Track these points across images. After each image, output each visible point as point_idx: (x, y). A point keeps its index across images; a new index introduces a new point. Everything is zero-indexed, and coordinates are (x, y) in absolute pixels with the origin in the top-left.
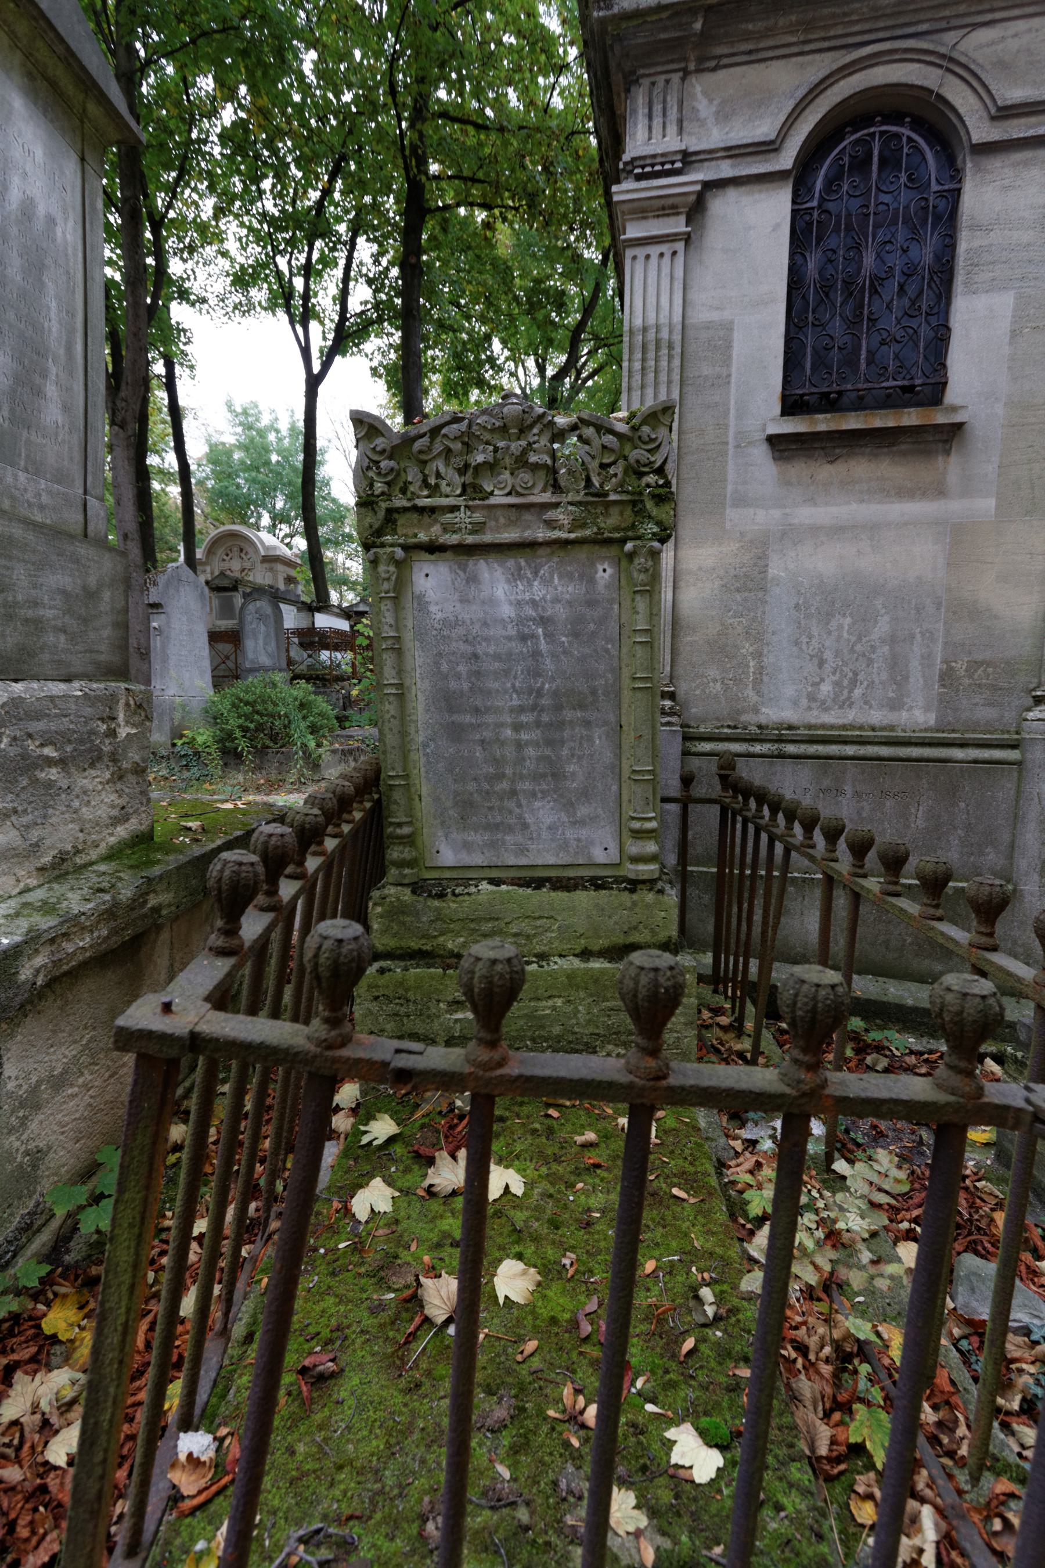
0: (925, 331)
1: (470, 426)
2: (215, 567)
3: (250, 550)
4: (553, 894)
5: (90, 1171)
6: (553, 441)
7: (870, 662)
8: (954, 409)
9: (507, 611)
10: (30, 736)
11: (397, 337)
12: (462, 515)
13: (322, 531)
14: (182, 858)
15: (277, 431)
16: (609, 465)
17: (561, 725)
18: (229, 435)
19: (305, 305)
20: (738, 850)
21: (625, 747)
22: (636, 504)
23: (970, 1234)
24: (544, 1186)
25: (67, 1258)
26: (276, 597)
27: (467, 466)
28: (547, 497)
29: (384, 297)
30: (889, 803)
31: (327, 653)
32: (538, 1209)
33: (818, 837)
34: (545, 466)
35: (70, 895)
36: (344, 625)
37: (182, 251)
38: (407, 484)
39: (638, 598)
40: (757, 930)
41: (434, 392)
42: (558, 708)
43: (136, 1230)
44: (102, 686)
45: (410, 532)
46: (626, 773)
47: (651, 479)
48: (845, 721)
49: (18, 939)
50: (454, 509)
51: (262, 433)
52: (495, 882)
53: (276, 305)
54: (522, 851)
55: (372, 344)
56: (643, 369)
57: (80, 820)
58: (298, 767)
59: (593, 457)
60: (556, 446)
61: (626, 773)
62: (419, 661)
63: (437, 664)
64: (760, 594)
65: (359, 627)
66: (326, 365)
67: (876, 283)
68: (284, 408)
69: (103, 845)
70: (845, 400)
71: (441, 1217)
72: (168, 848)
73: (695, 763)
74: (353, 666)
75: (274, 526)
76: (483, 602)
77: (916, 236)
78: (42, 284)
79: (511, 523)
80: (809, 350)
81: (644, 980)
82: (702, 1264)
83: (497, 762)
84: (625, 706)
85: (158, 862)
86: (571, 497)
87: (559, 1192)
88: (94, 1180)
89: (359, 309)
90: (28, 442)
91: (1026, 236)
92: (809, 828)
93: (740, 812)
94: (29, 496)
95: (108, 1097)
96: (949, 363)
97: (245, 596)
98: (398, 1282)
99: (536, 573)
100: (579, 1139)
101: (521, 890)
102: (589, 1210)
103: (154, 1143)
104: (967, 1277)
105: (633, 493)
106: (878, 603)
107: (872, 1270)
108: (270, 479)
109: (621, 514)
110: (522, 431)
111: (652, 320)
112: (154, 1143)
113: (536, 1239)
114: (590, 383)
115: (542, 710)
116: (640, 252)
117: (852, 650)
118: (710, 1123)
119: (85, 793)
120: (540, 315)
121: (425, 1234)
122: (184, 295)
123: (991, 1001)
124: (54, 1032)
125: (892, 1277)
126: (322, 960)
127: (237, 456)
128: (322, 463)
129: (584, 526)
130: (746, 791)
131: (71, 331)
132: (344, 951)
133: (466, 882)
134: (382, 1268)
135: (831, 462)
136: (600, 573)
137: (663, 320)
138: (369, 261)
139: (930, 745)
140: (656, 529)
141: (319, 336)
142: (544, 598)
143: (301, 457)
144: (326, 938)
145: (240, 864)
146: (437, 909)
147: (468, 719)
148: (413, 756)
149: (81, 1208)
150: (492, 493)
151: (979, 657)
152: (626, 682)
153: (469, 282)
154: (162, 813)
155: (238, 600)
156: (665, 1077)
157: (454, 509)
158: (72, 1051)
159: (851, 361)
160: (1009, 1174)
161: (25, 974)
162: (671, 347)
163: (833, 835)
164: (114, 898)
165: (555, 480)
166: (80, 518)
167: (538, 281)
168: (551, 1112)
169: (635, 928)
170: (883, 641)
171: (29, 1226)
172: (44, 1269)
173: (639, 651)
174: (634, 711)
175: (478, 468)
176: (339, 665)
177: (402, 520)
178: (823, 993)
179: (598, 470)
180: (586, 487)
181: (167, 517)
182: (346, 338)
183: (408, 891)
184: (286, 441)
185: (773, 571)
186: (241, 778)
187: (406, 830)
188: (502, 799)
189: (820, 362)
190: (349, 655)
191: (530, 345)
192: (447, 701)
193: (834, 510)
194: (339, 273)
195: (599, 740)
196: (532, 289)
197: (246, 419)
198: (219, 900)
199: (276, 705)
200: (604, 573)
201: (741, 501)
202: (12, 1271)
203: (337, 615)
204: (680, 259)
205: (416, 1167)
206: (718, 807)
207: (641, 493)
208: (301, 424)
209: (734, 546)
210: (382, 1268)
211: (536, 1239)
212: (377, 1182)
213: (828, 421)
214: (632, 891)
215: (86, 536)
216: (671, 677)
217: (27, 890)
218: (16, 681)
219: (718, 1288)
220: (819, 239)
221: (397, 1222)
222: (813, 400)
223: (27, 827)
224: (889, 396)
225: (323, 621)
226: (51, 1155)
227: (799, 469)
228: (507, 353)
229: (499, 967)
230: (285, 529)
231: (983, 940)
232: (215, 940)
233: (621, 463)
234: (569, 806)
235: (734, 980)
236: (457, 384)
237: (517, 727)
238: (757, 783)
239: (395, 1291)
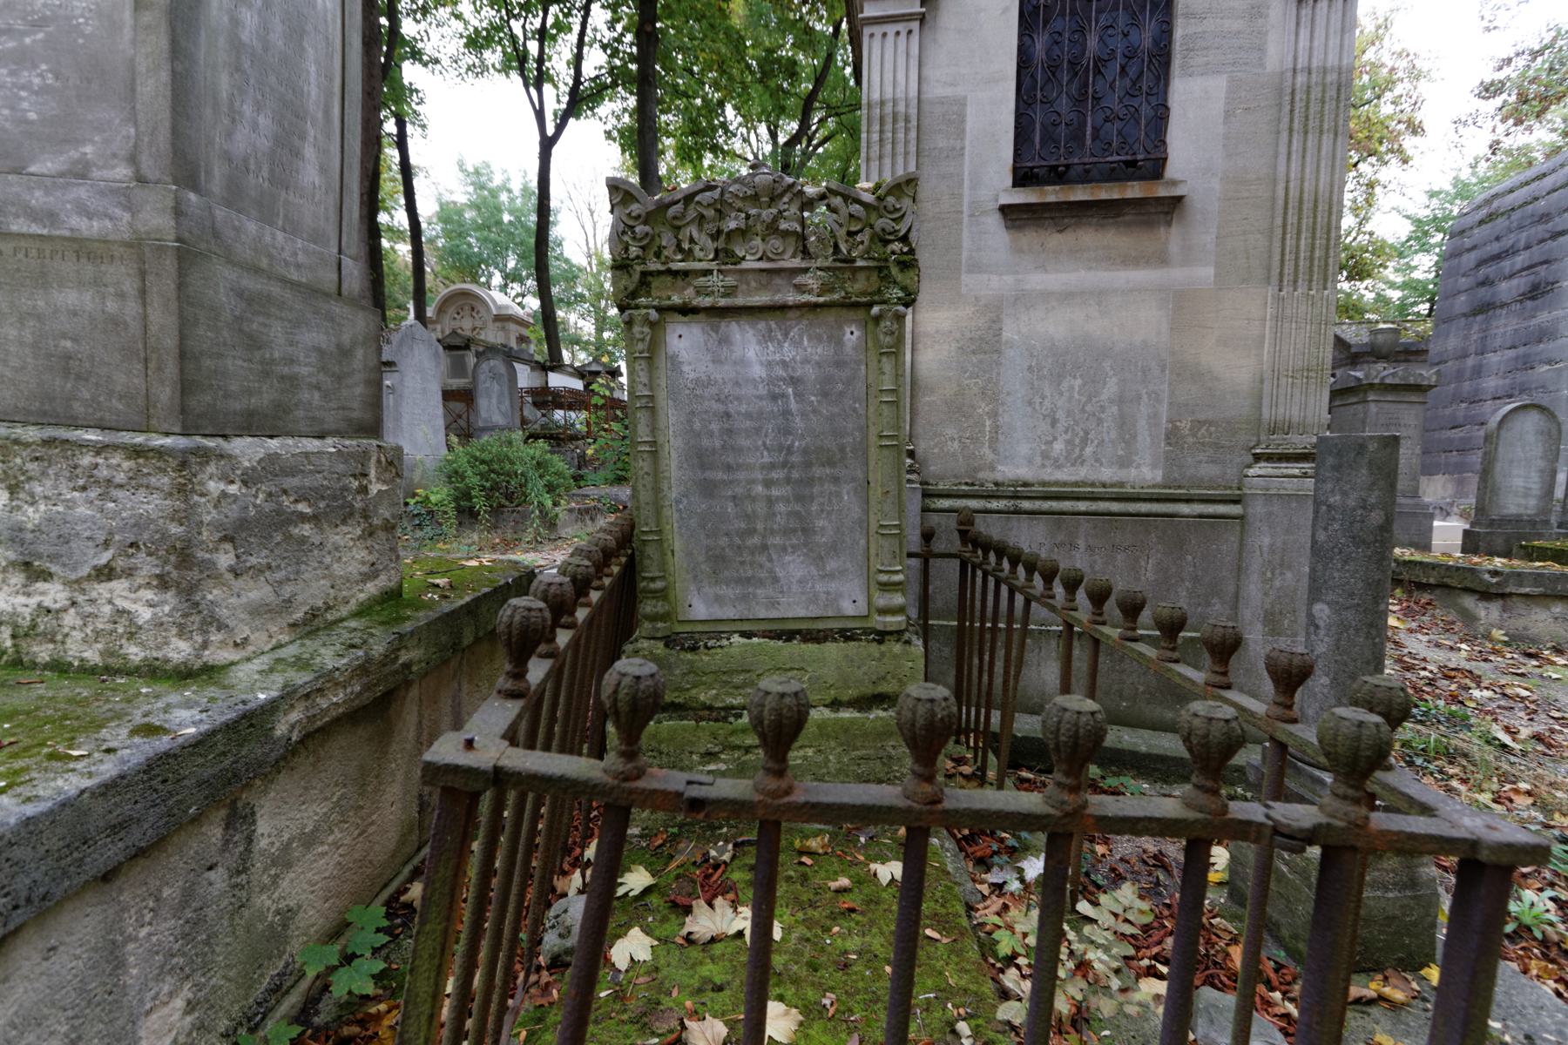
0: (1146, 111)
1: (722, 194)
2: (446, 326)
3: (482, 310)
5: (339, 930)
6: (802, 210)
7: (1100, 421)
8: (1174, 183)
9: (758, 371)
10: (285, 492)
11: (632, 102)
12: (715, 280)
13: (555, 290)
14: (433, 615)
15: (509, 191)
16: (856, 233)
17: (810, 482)
18: (461, 195)
19: (539, 69)
20: (978, 604)
21: (872, 502)
22: (881, 270)
23: (1207, 968)
24: (801, 930)
25: (317, 1020)
27: (719, 232)
28: (797, 262)
29: (618, 62)
30: (1120, 557)
31: (561, 412)
32: (796, 952)
33: (1058, 589)
34: (795, 233)
35: (323, 651)
36: (578, 385)
37: (415, 12)
38: (660, 249)
39: (884, 359)
40: (998, 681)
41: (670, 154)
42: (808, 465)
43: (436, 961)
44: (354, 443)
46: (873, 527)
47: (896, 246)
48: (1078, 478)
49: (274, 694)
51: (494, 194)
52: (747, 635)
53: (511, 68)
54: (774, 604)
55: (606, 108)
56: (881, 140)
57: (331, 576)
58: (534, 525)
59: (841, 225)
60: (806, 214)
61: (873, 527)
62: (672, 420)
63: (689, 421)
64: (995, 356)
65: (594, 386)
66: (560, 128)
67: (1100, 64)
68: (515, 168)
69: (353, 601)
70: (1072, 173)
71: (701, 963)
72: (417, 604)
73: (934, 519)
74: (588, 424)
75: (506, 285)
77: (1135, 22)
78: (303, 49)
79: (763, 287)
80: (1038, 126)
81: (921, 710)
82: (957, 1000)
83: (749, 518)
84: (872, 463)
85: (408, 618)
86: (819, 262)
87: (816, 936)
88: (342, 941)
89: (593, 74)
90: (287, 202)
91: (1237, 25)
92: (1048, 579)
93: (980, 566)
94: (286, 255)
95: (357, 856)
96: (1169, 139)
97: (478, 355)
98: (662, 1027)
99: (786, 335)
100: (833, 885)
102: (846, 952)
103: (456, 875)
104: (1206, 1009)
105: (879, 260)
106: (1107, 364)
107: (1121, 998)
108: (502, 238)
109: (868, 279)
111: (889, 95)
112: (456, 875)
113: (796, 981)
114: (820, 150)
115: (792, 467)
116: (878, 30)
117: (1083, 411)
118: (957, 869)
119: (337, 549)
120: (772, 84)
121: (686, 980)
122: (416, 55)
123: (1234, 724)
124: (306, 789)
125: (1140, 1004)
126: (621, 696)
127: (469, 215)
128: (555, 224)
129: (832, 290)
130: (986, 546)
131: (329, 95)
132: (642, 687)
133: (718, 635)
134: (645, 1014)
135: (1060, 231)
136: (848, 335)
137: (900, 94)
138: (603, 28)
139: (1158, 500)
140: (901, 294)
141: (554, 99)
142: (794, 359)
143: (534, 218)
144: (624, 675)
145: (530, 610)
146: (690, 662)
147: (720, 475)
148: (667, 512)
149: (332, 969)
150: (743, 258)
151: (1202, 417)
152: (873, 439)
153: (703, 50)
154: (407, 570)
155: (471, 359)
156: (940, 801)
158: (322, 809)
159: (1077, 136)
160: (1246, 913)
161: (281, 730)
162: (907, 120)
163: (1072, 585)
164: (366, 654)
165: (805, 246)
166: (335, 276)
167: (770, 51)
168: (804, 859)
169: (884, 678)
170: (1111, 401)
171: (279, 987)
172: (296, 1030)
173: (886, 410)
174: (880, 469)
175: (730, 234)
176: (573, 425)
178: (1084, 719)
180: (834, 253)
181: (395, 275)
182: (580, 100)
183: (661, 644)
184: (519, 201)
185: (1006, 335)
186: (475, 537)
187: (659, 585)
188: (753, 554)
189: (1048, 138)
190: (584, 415)
191: (763, 112)
192: (700, 458)
193: (1064, 277)
194: (573, 38)
195: (847, 495)
196: (765, 59)
197: (478, 178)
198: (509, 644)
200: (852, 335)
201: (976, 268)
202: (261, 1033)
203: (571, 375)
204: (915, 37)
205: (673, 917)
206: (957, 562)
207: (886, 260)
208: (534, 184)
210: (645, 1014)
211: (796, 981)
212: (636, 932)
213: (1057, 192)
214: (880, 642)
215: (340, 294)
216: (911, 436)
217: (279, 646)
218: (271, 437)
219: (973, 1022)
220: (1046, 22)
221: (657, 969)
222: (1041, 172)
223: (280, 583)
224: (1113, 170)
225: (556, 380)
226: (301, 915)
227: (1029, 237)
228: (740, 119)
229: (787, 700)
230: (516, 288)
231: (1218, 679)
232: (502, 682)
233: (868, 231)
234: (819, 560)
235: (976, 730)
236: (690, 148)
237: (768, 484)
238: (996, 538)
239: (659, 1035)
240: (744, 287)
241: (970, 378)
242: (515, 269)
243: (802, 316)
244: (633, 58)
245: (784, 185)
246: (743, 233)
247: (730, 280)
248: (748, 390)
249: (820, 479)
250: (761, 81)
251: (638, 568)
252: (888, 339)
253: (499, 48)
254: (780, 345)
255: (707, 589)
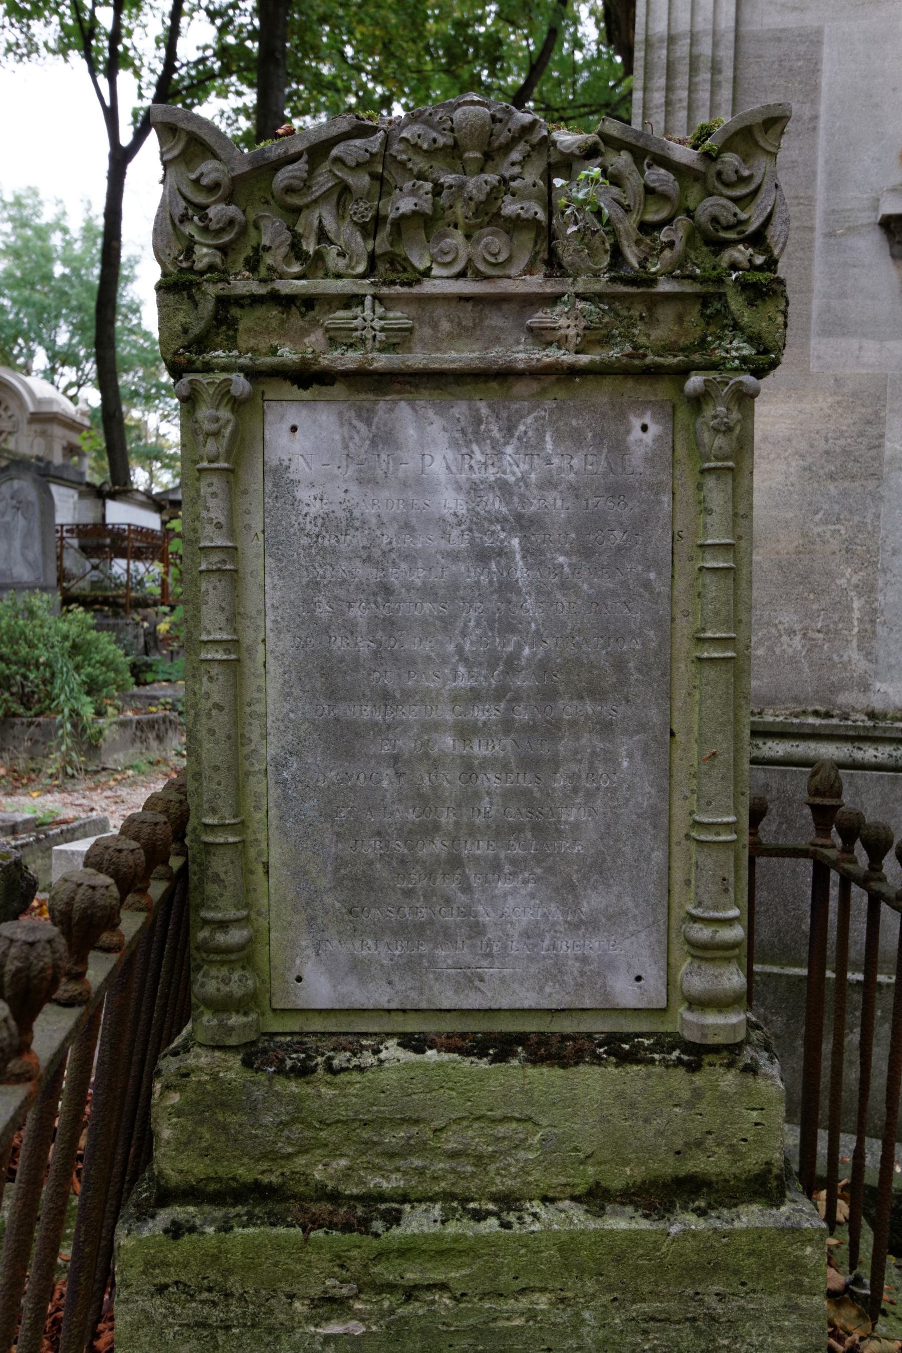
1: (387, 143)
4: (531, 1071)
9: (451, 502)
11: (250, 98)
13: (127, 380)
15: (65, 231)
17: (552, 729)
19: (113, 49)
22: (709, 302)
26: (45, 474)
27: (378, 220)
28: (535, 283)
29: (231, 40)
34: (534, 222)
36: (151, 521)
38: (259, 250)
39: (710, 482)
42: (549, 695)
45: (263, 344)
46: (680, 826)
47: (741, 253)
50: (352, 301)
52: (415, 1043)
53: (69, 46)
54: (471, 979)
56: (668, 103)
59: (627, 210)
61: (680, 826)
63: (308, 602)
64: (871, 485)
68: (76, 201)
74: (164, 584)
75: (53, 370)
76: (405, 485)
79: (463, 332)
84: (680, 694)
86: (582, 285)
99: (509, 430)
101: (466, 1063)
105: (704, 281)
109: (680, 319)
110: (488, 156)
115: (516, 699)
129: (606, 341)
130: (852, 831)
133: (353, 1042)
136: (637, 433)
137: (703, 24)
140: (748, 351)
141: (133, 93)
142: (524, 479)
147: (367, 713)
148: (256, 785)
150: (427, 273)
152: (683, 645)
153: (361, 22)
157: (352, 301)
162: (715, 69)
165: (552, 251)
167: (461, 25)
169: (699, 1144)
173: (713, 587)
176: (141, 583)
177: (246, 320)
179: (635, 234)
180: (612, 267)
183: (235, 1061)
184: (78, 247)
187: (236, 936)
188: (430, 875)
190: (157, 568)
192: (328, 677)
199: (32, 646)
200: (644, 433)
201: (837, 326)
203: (142, 505)
207: (719, 281)
208: (100, 222)
209: (825, 402)
214: (693, 1068)
225: (118, 514)
230: (69, 374)
233: (682, 221)
234: (567, 891)
237: (466, 732)
240: (427, 331)
241: (826, 522)
242: (70, 345)
243: (543, 391)
244: (252, 36)
245: (514, 126)
246: (427, 223)
247: (398, 317)
248: (428, 541)
249: (573, 723)
250: (447, 71)
251: (194, 898)
252: (720, 441)
253: (55, 19)
255: (334, 946)
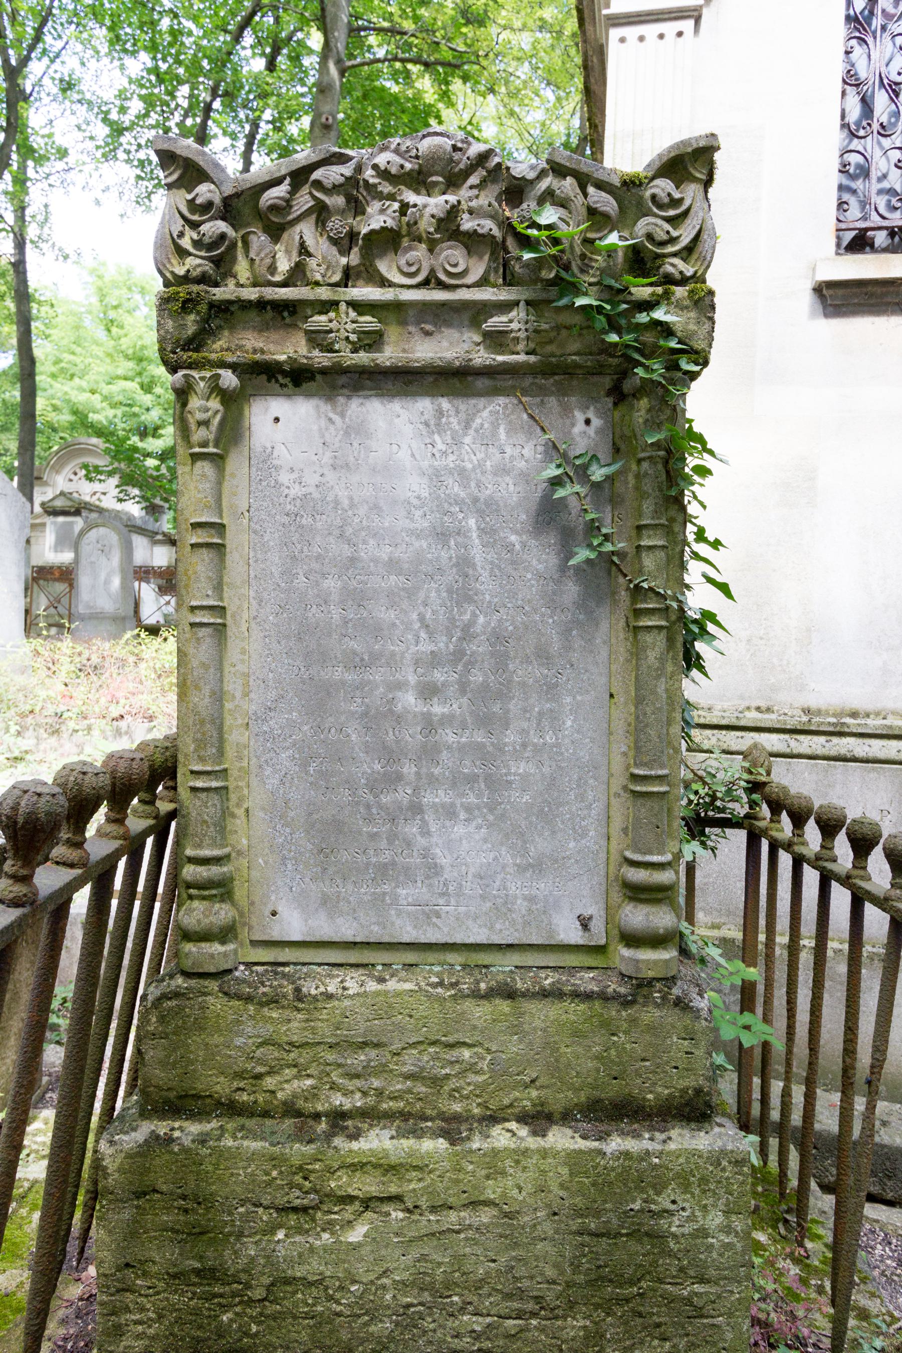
9: (415, 486)
27: (353, 236)
83: (391, 755)
92: (799, 820)
93: (788, 846)
116: (631, 32)
142: (481, 464)
147: (338, 673)
237: (428, 691)
254: (457, 442)
